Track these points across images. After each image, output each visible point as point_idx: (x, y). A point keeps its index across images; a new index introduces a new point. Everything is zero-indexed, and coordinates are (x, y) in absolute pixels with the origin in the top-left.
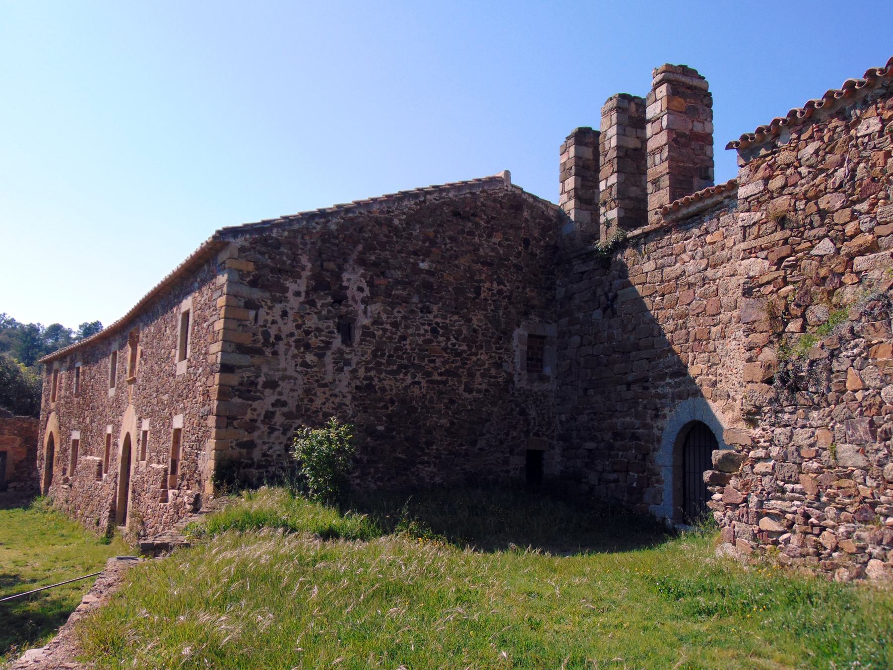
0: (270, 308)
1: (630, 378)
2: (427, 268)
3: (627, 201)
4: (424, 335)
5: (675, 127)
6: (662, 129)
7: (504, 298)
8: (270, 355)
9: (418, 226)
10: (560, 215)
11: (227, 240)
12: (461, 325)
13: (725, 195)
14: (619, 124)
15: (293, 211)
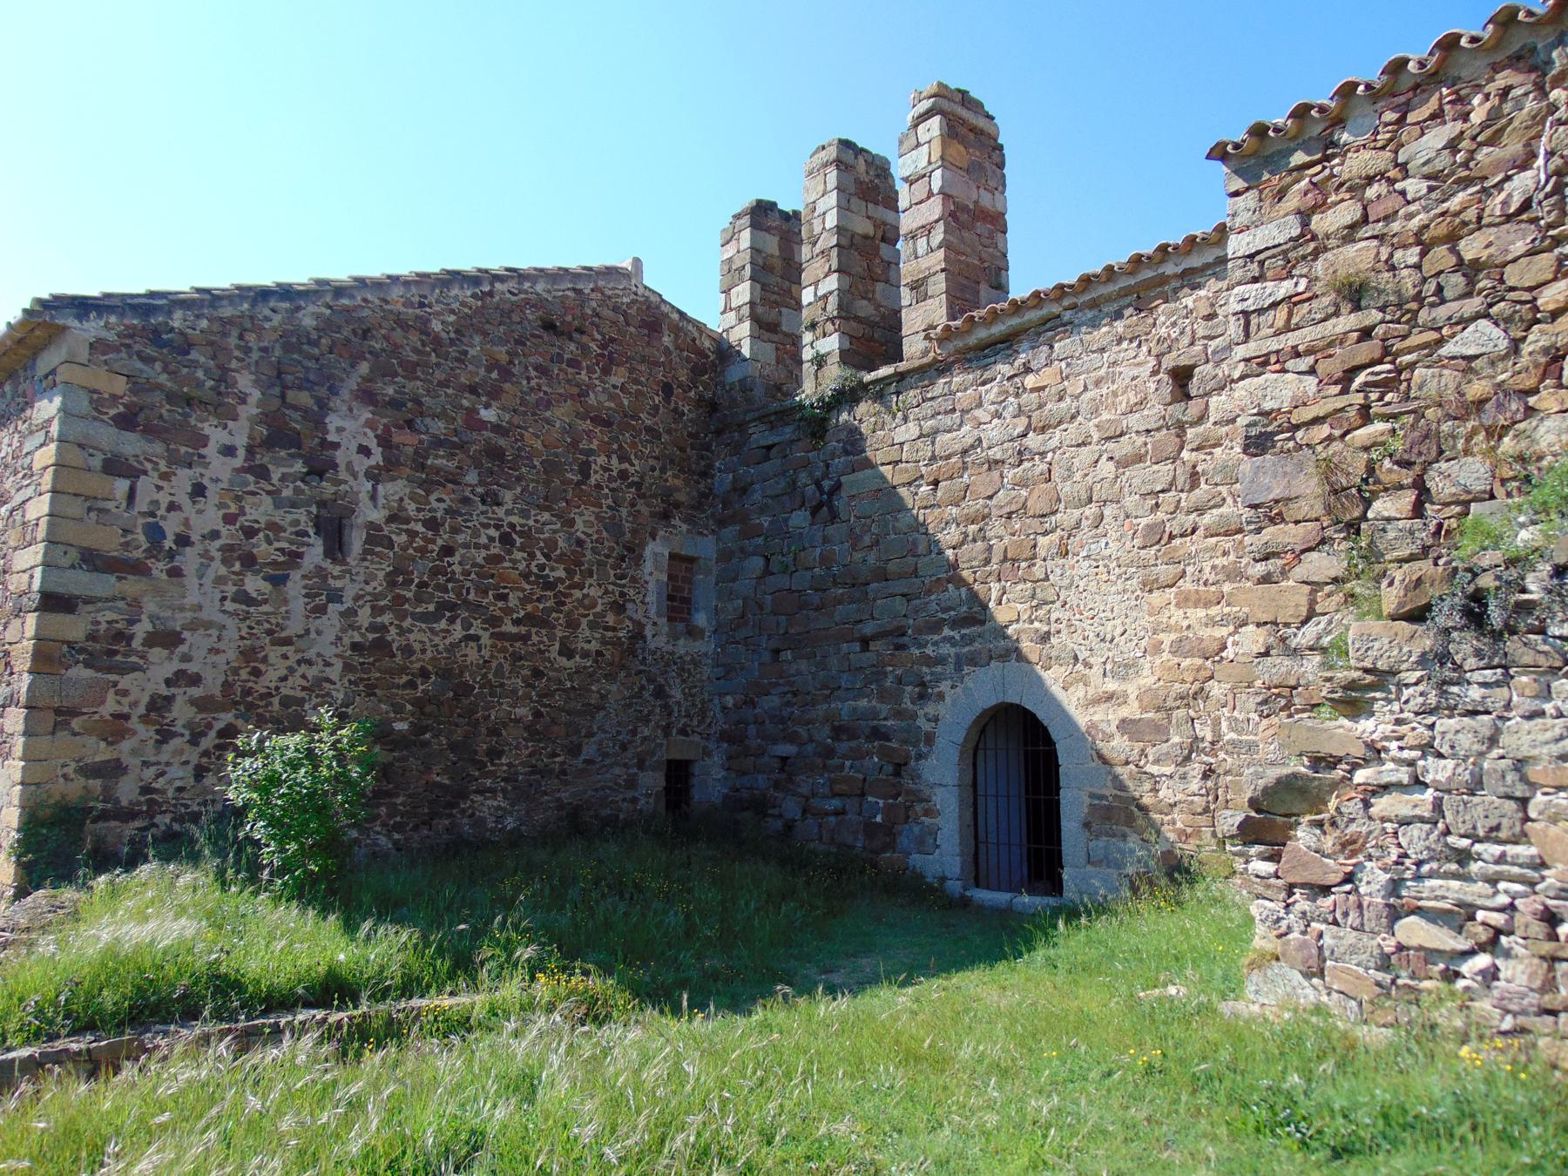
0: (165, 476)
1: (869, 629)
2: (493, 419)
3: (854, 324)
4: (486, 547)
5: (954, 193)
6: (930, 194)
7: (630, 486)
8: (164, 576)
9: (477, 339)
10: (724, 352)
11: (60, 322)
12: (555, 532)
13: (1066, 303)
14: (840, 189)
15: (221, 279)
